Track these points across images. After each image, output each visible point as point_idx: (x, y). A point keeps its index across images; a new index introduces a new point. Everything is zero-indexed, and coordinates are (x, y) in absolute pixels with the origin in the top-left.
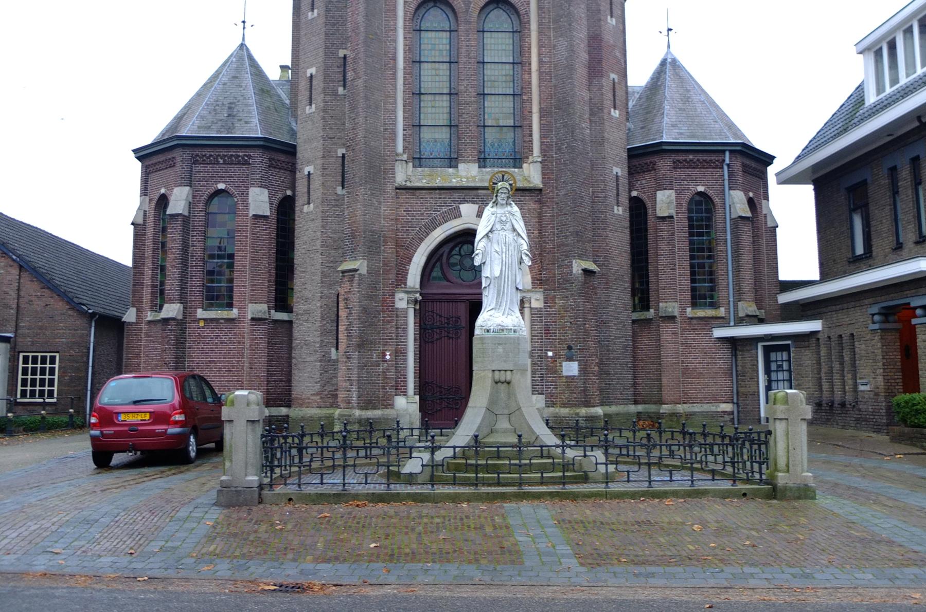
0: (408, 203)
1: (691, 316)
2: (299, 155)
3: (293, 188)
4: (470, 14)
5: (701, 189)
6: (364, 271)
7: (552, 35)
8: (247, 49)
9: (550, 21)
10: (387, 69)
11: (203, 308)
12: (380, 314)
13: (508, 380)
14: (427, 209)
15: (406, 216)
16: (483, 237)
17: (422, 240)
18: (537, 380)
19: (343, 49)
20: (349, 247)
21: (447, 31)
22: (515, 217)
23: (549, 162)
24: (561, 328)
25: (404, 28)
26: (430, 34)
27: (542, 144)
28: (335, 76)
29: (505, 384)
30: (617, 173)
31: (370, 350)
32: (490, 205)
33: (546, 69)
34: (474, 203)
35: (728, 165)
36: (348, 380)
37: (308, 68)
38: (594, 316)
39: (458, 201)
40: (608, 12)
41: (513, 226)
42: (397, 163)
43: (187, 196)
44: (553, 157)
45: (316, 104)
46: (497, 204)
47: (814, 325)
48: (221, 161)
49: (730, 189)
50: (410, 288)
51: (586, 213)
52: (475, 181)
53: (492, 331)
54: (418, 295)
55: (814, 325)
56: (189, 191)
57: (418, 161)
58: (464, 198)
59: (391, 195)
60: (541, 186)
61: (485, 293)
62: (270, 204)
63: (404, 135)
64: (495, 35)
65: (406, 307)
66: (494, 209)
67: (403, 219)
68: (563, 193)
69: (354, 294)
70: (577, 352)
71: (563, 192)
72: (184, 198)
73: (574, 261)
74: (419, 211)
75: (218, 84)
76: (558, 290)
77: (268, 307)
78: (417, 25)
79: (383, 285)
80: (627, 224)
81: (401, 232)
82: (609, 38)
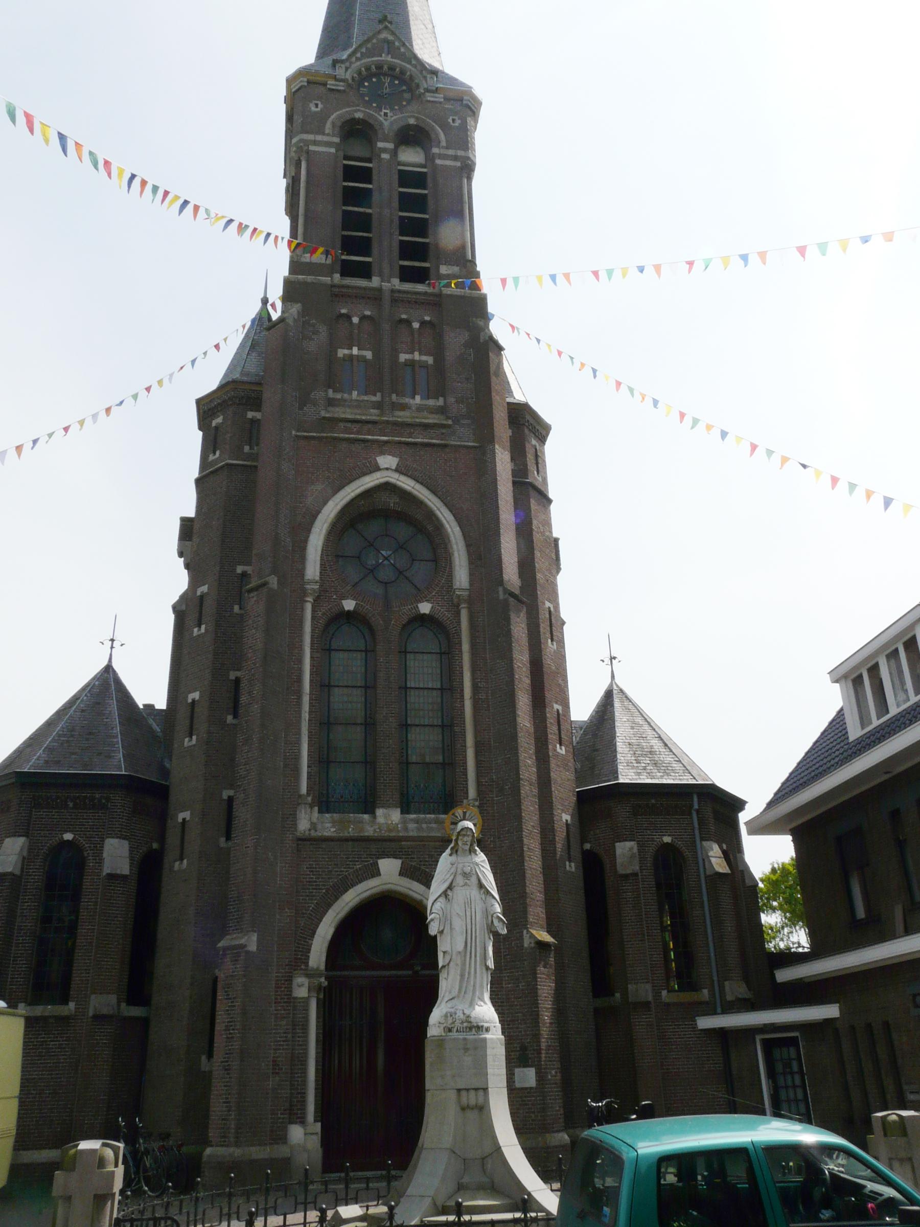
0: (312, 858)
1: (667, 1000)
2: (173, 798)
3: (162, 839)
5: (667, 839)
6: (253, 947)
8: (114, 671)
11: (25, 1002)
14: (337, 865)
15: (309, 875)
16: (440, 896)
17: (329, 906)
19: (235, 670)
21: (363, 651)
26: (341, 655)
27: (479, 784)
29: (476, 1112)
30: (567, 821)
32: (448, 851)
35: (698, 811)
37: (190, 692)
40: (548, 635)
41: (479, 880)
43: (21, 850)
45: (197, 736)
46: (457, 851)
47: (830, 1011)
48: (71, 805)
49: (702, 839)
50: (313, 969)
53: (455, 1029)
54: (323, 980)
55: (830, 1011)
56: (24, 843)
57: (325, 804)
58: (384, 852)
61: (442, 976)
62: (131, 860)
64: (420, 656)
66: (454, 858)
69: (238, 980)
72: (17, 852)
75: (75, 711)
76: (505, 969)
77: (118, 998)
78: (326, 644)
81: (302, 896)
82: (548, 662)
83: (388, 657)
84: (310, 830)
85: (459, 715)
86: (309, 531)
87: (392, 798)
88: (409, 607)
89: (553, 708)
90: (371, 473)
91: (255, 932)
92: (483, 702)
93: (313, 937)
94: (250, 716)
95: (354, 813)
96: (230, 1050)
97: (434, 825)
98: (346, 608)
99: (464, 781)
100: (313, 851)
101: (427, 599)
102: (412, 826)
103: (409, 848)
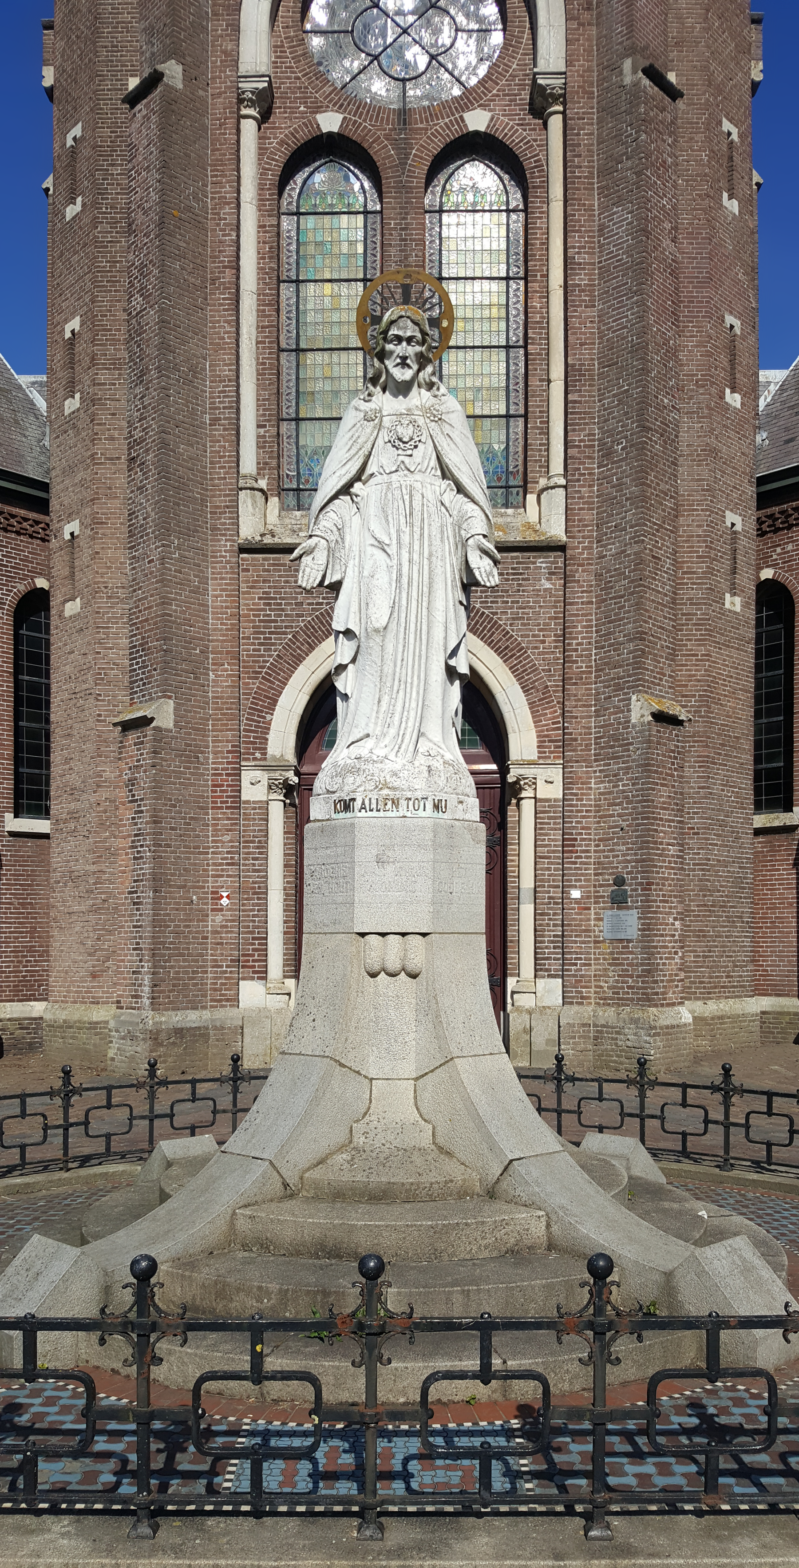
4: (409, 171)
9: (592, 173)
10: (218, 288)
12: (207, 814)
13: (411, 967)
15: (265, 610)
17: (299, 660)
18: (547, 947)
20: (138, 675)
21: (359, 213)
22: (447, 429)
23: (583, 486)
24: (599, 840)
30: (733, 525)
31: (184, 887)
36: (134, 949)
37: (66, 321)
38: (676, 816)
42: (242, 494)
44: (594, 474)
50: (274, 758)
51: (666, 595)
59: (228, 562)
60: (565, 539)
63: (258, 437)
65: (265, 798)
67: (259, 615)
69: (145, 771)
70: (636, 890)
73: (634, 698)
74: (292, 598)
76: (596, 760)
79: (215, 753)
80: (751, 633)
88: (447, 120)
89: (723, 321)
91: (170, 697)
92: (584, 291)
93: (274, 710)
96: (138, 875)
100: (269, 571)
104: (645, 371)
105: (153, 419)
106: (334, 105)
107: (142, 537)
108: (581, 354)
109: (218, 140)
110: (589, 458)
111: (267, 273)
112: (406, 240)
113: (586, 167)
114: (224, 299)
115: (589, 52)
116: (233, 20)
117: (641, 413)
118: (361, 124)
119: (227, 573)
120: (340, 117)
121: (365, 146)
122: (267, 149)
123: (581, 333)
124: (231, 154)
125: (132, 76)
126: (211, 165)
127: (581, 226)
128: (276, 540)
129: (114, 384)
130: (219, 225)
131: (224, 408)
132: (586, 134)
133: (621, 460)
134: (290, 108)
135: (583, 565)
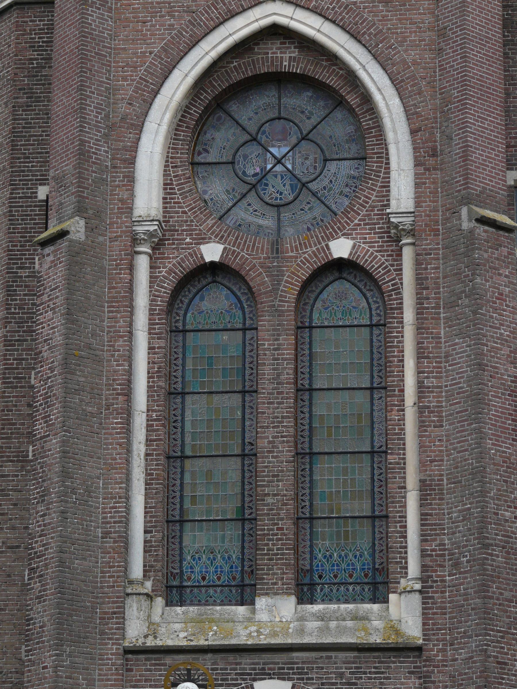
0: (151, 680)
4: (281, 296)
7: (442, 333)
10: (111, 414)
23: (436, 592)
25: (150, 329)
28: (23, 424)
33: (429, 402)
34: (284, 679)
39: (250, 674)
44: (445, 581)
52: (287, 634)
58: (263, 669)
63: (145, 542)
68: (463, 656)
71: (463, 654)
83: (277, 340)
84: (146, 637)
85: (396, 434)
86: (139, 128)
87: (282, 579)
90: (244, 10)
92: (433, 412)
94: (47, 456)
95: (222, 604)
97: (349, 624)
98: (208, 259)
99: (401, 547)
100: (150, 670)
101: (345, 231)
102: (313, 625)
103: (303, 663)
104: (483, 493)
105: (52, 538)
106: (216, 237)
107: (38, 643)
108: (431, 470)
109: (113, 279)
110: (441, 566)
111: (155, 391)
112: (278, 359)
113: (433, 298)
114: (117, 423)
115: (435, 193)
116: (129, 172)
117: (482, 529)
118: (239, 253)
119: (112, 674)
120: (221, 247)
121: (243, 273)
122: (157, 277)
123: (431, 451)
124: (126, 292)
125: (41, 184)
126: (108, 302)
127: (430, 353)
128: (159, 643)
129: (17, 476)
130: (113, 356)
131: (115, 522)
132: (432, 269)
133: (466, 572)
134: (177, 240)
135: (438, 666)
